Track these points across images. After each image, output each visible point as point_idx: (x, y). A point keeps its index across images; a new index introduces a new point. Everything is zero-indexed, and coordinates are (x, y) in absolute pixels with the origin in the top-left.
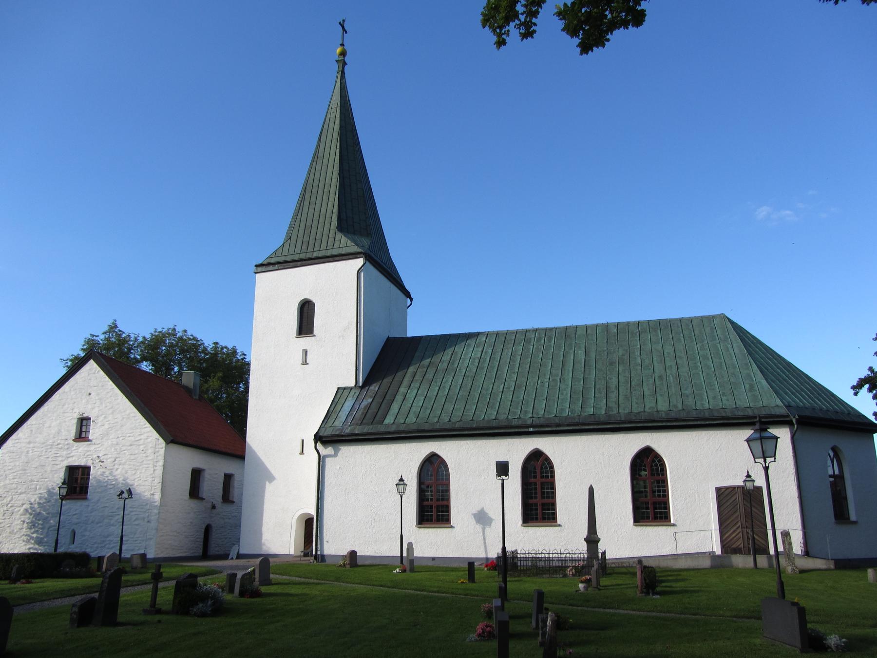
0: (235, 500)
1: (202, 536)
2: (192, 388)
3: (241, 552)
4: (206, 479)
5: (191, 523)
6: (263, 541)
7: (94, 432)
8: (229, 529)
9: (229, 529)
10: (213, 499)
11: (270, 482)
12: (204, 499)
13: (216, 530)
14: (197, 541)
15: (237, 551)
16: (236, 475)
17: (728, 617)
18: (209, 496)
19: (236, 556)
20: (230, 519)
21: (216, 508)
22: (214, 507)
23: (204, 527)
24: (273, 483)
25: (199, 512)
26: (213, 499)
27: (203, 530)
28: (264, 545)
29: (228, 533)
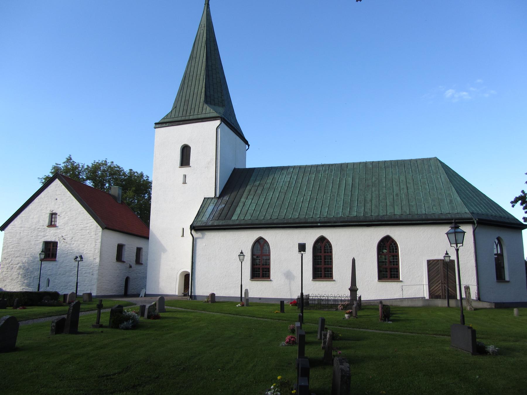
1: (124, 283)
7: (59, 222)
12: (125, 262)
13: (132, 280)
16: (143, 248)
20: (140, 273)
21: (132, 267)
22: (131, 267)
23: (125, 278)
27: (125, 280)
29: (139, 282)
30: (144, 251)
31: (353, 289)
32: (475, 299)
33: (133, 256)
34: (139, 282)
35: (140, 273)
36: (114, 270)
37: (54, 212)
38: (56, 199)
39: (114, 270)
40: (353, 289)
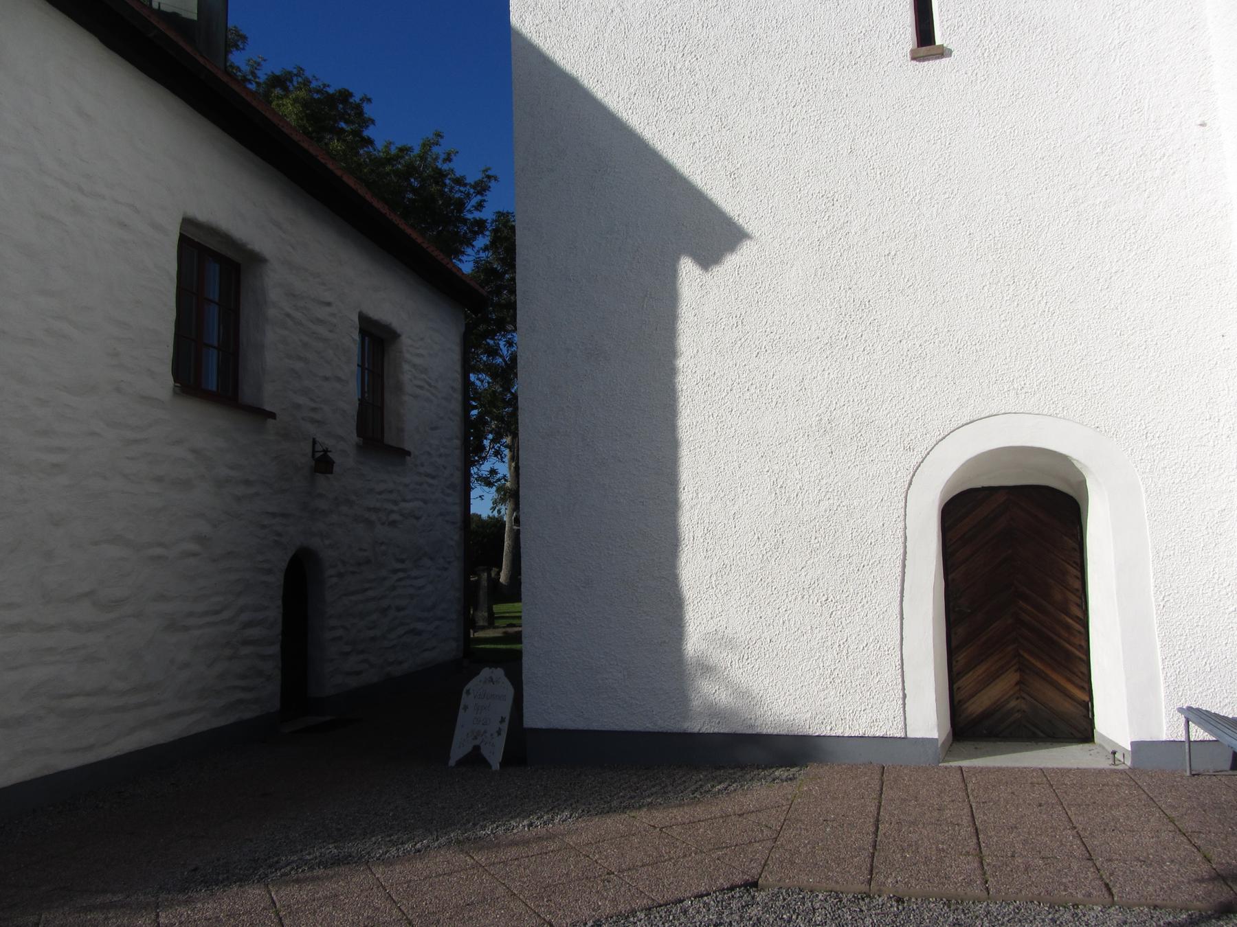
0: (408, 446)
1: (274, 612)
2: (195, 17)
3: (532, 720)
4: (272, 312)
5: (200, 539)
6: (695, 641)
7: (500, 719)
8: (395, 571)
9: (395, 571)
10: (313, 421)
11: (708, 260)
12: (272, 415)
13: (340, 575)
14: (246, 643)
15: (505, 708)
16: (405, 340)
17: (1080, 678)
18: (298, 407)
19: (500, 743)
20: (393, 524)
21: (336, 468)
22: (323, 463)
23: (281, 560)
24: (732, 261)
25: (247, 483)
26: (313, 421)
27: (277, 579)
28: (707, 669)
29: (394, 588)
30: (407, 356)
31: (159, 7)
32: (933, 733)
33: (339, 379)
34: (394, 588)
35: (393, 524)
36: (159, 479)
37: (441, 134)
38: (1203, 125)
39: (159, 479)
40: (159, 7)
